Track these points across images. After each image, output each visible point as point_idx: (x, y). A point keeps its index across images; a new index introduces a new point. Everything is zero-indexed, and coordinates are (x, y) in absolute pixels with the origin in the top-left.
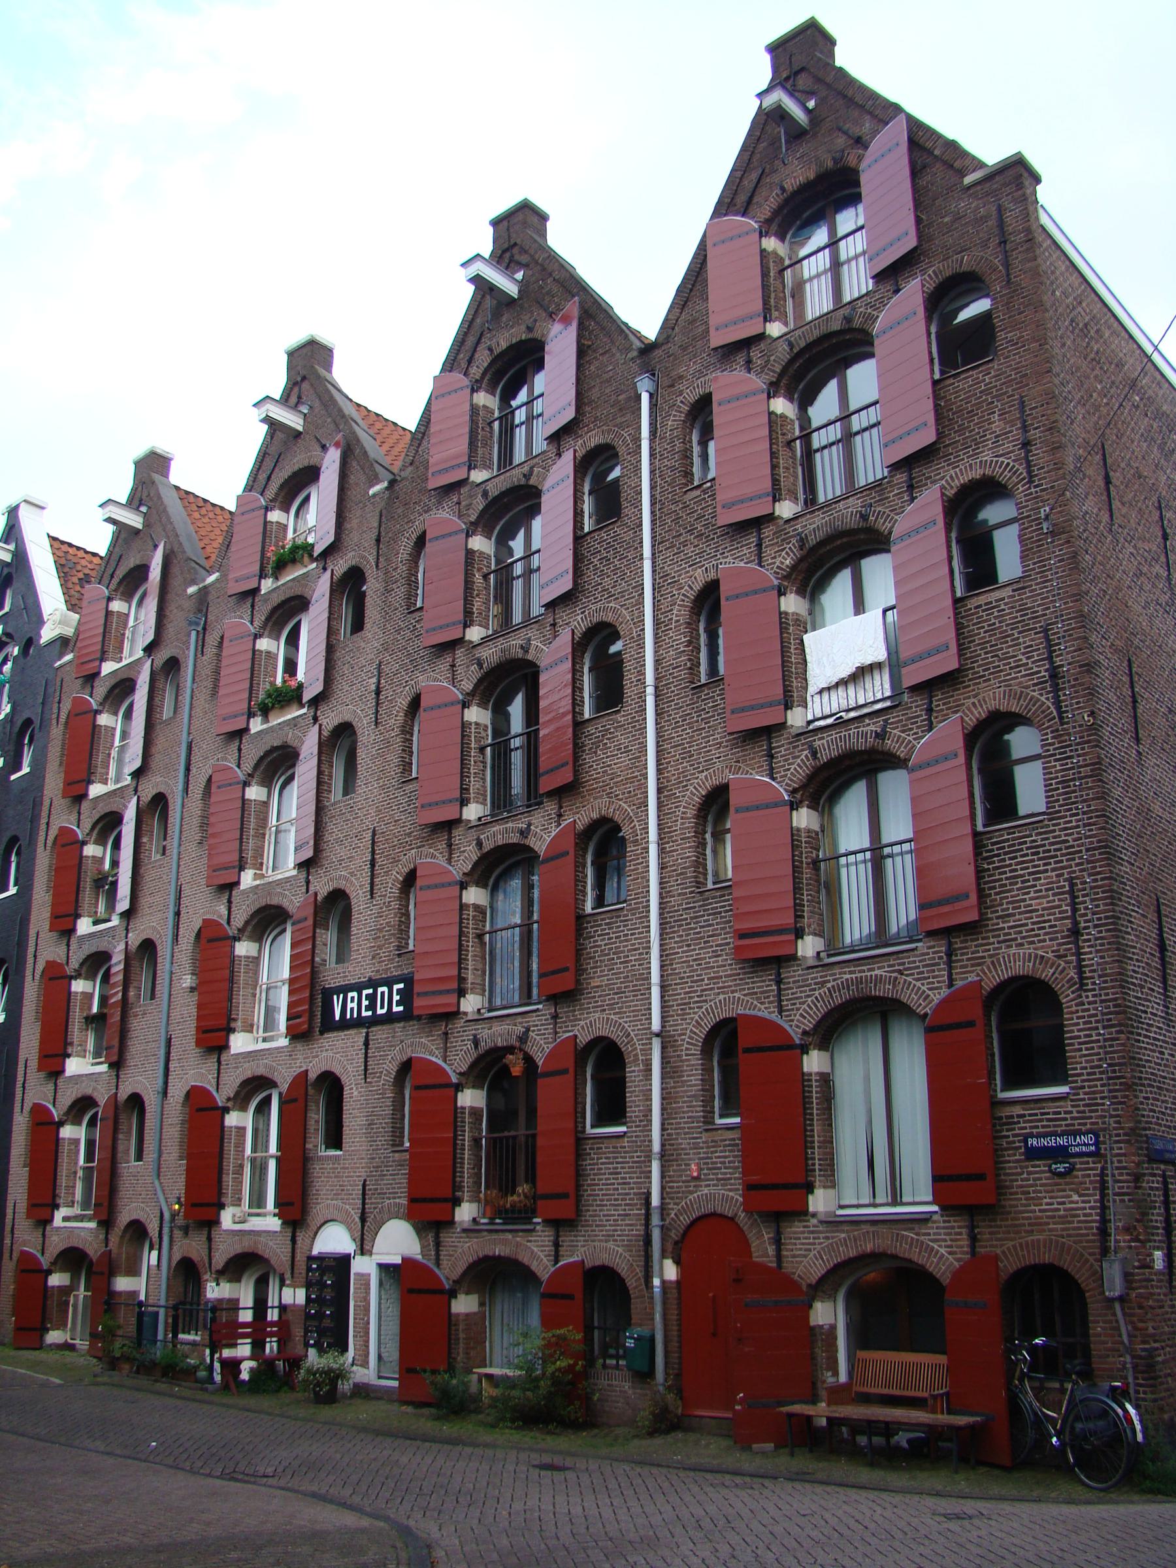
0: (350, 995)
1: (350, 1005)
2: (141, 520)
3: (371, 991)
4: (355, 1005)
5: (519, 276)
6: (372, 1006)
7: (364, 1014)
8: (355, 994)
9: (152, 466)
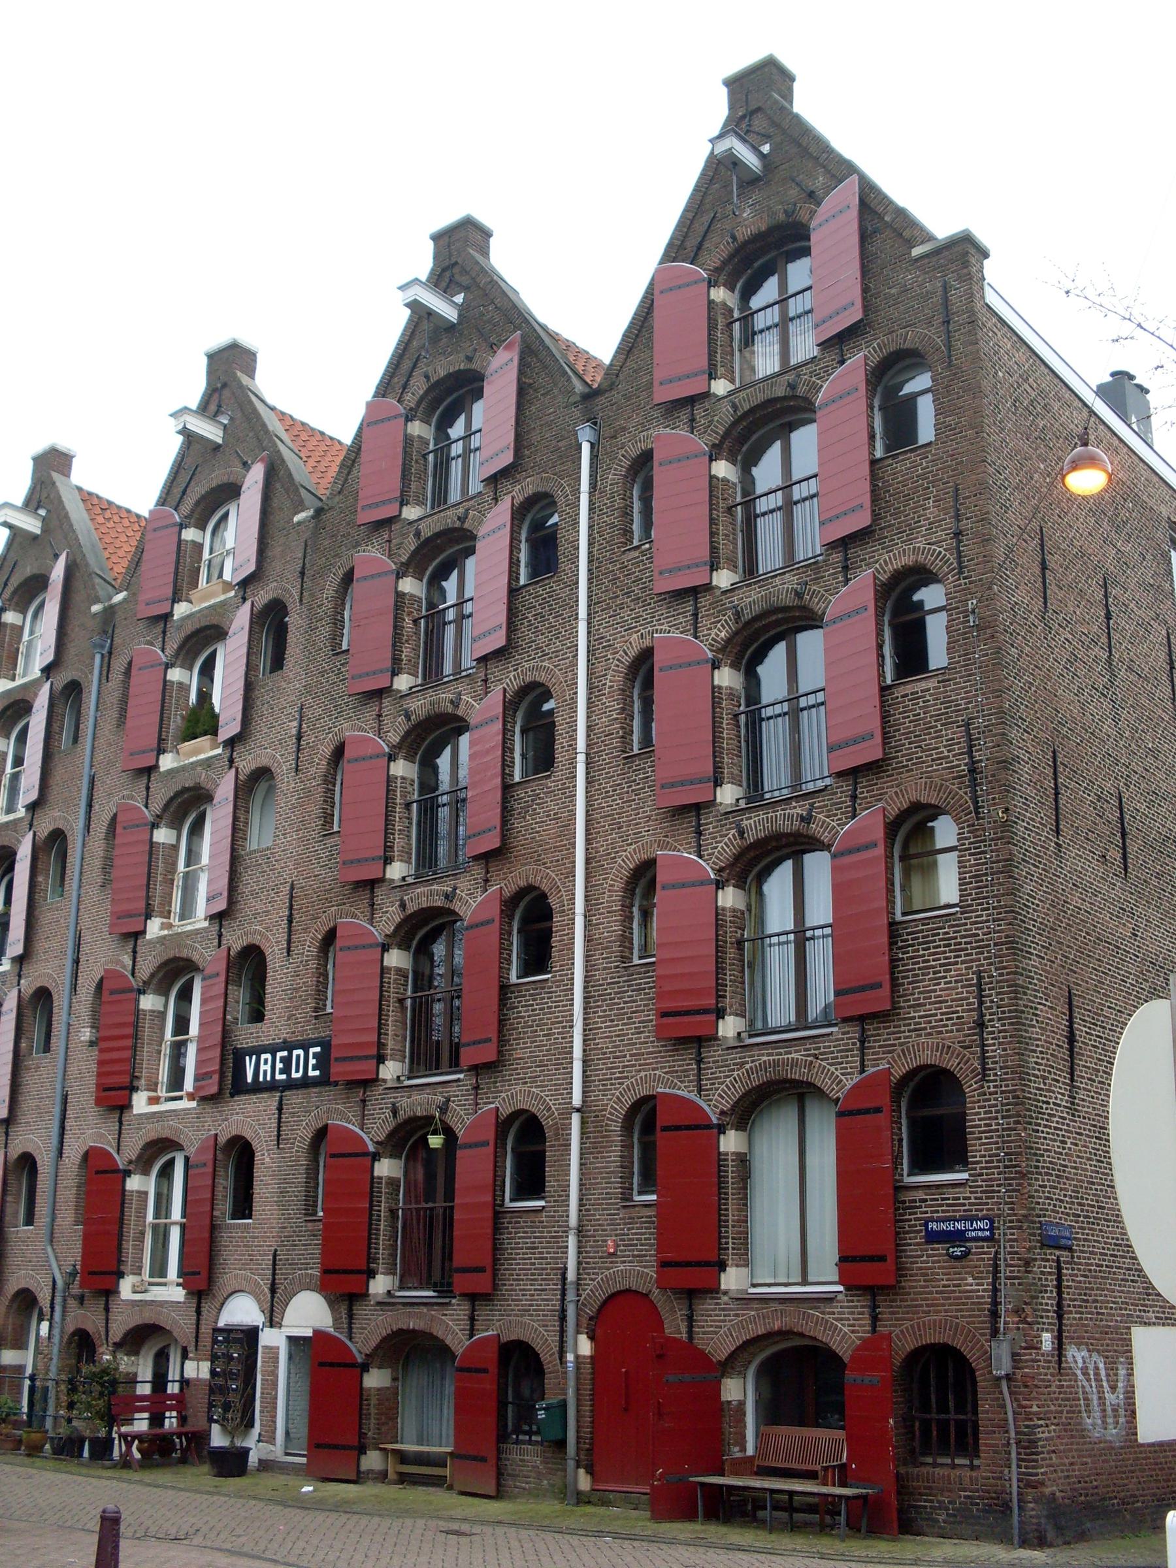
0: (263, 1056)
1: (263, 1067)
2: (39, 524)
3: (285, 1053)
4: (268, 1067)
5: (459, 299)
6: (286, 1070)
7: (278, 1077)
8: (269, 1056)
9: (52, 464)
